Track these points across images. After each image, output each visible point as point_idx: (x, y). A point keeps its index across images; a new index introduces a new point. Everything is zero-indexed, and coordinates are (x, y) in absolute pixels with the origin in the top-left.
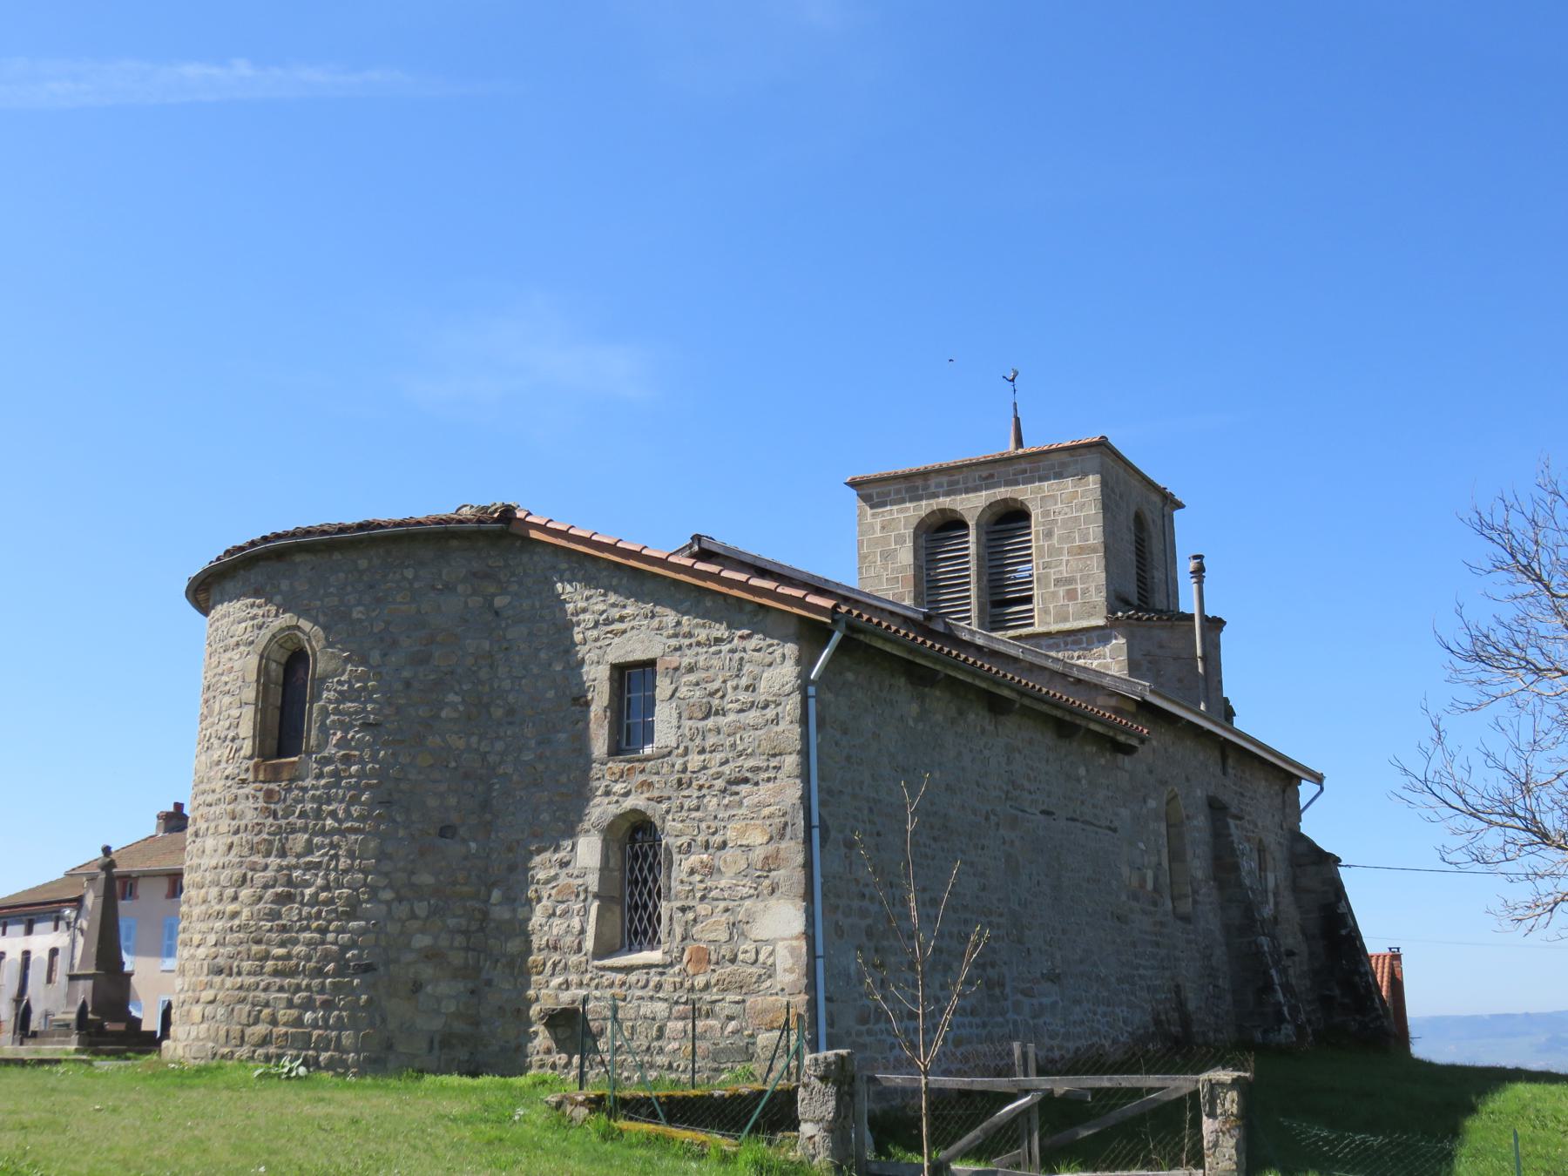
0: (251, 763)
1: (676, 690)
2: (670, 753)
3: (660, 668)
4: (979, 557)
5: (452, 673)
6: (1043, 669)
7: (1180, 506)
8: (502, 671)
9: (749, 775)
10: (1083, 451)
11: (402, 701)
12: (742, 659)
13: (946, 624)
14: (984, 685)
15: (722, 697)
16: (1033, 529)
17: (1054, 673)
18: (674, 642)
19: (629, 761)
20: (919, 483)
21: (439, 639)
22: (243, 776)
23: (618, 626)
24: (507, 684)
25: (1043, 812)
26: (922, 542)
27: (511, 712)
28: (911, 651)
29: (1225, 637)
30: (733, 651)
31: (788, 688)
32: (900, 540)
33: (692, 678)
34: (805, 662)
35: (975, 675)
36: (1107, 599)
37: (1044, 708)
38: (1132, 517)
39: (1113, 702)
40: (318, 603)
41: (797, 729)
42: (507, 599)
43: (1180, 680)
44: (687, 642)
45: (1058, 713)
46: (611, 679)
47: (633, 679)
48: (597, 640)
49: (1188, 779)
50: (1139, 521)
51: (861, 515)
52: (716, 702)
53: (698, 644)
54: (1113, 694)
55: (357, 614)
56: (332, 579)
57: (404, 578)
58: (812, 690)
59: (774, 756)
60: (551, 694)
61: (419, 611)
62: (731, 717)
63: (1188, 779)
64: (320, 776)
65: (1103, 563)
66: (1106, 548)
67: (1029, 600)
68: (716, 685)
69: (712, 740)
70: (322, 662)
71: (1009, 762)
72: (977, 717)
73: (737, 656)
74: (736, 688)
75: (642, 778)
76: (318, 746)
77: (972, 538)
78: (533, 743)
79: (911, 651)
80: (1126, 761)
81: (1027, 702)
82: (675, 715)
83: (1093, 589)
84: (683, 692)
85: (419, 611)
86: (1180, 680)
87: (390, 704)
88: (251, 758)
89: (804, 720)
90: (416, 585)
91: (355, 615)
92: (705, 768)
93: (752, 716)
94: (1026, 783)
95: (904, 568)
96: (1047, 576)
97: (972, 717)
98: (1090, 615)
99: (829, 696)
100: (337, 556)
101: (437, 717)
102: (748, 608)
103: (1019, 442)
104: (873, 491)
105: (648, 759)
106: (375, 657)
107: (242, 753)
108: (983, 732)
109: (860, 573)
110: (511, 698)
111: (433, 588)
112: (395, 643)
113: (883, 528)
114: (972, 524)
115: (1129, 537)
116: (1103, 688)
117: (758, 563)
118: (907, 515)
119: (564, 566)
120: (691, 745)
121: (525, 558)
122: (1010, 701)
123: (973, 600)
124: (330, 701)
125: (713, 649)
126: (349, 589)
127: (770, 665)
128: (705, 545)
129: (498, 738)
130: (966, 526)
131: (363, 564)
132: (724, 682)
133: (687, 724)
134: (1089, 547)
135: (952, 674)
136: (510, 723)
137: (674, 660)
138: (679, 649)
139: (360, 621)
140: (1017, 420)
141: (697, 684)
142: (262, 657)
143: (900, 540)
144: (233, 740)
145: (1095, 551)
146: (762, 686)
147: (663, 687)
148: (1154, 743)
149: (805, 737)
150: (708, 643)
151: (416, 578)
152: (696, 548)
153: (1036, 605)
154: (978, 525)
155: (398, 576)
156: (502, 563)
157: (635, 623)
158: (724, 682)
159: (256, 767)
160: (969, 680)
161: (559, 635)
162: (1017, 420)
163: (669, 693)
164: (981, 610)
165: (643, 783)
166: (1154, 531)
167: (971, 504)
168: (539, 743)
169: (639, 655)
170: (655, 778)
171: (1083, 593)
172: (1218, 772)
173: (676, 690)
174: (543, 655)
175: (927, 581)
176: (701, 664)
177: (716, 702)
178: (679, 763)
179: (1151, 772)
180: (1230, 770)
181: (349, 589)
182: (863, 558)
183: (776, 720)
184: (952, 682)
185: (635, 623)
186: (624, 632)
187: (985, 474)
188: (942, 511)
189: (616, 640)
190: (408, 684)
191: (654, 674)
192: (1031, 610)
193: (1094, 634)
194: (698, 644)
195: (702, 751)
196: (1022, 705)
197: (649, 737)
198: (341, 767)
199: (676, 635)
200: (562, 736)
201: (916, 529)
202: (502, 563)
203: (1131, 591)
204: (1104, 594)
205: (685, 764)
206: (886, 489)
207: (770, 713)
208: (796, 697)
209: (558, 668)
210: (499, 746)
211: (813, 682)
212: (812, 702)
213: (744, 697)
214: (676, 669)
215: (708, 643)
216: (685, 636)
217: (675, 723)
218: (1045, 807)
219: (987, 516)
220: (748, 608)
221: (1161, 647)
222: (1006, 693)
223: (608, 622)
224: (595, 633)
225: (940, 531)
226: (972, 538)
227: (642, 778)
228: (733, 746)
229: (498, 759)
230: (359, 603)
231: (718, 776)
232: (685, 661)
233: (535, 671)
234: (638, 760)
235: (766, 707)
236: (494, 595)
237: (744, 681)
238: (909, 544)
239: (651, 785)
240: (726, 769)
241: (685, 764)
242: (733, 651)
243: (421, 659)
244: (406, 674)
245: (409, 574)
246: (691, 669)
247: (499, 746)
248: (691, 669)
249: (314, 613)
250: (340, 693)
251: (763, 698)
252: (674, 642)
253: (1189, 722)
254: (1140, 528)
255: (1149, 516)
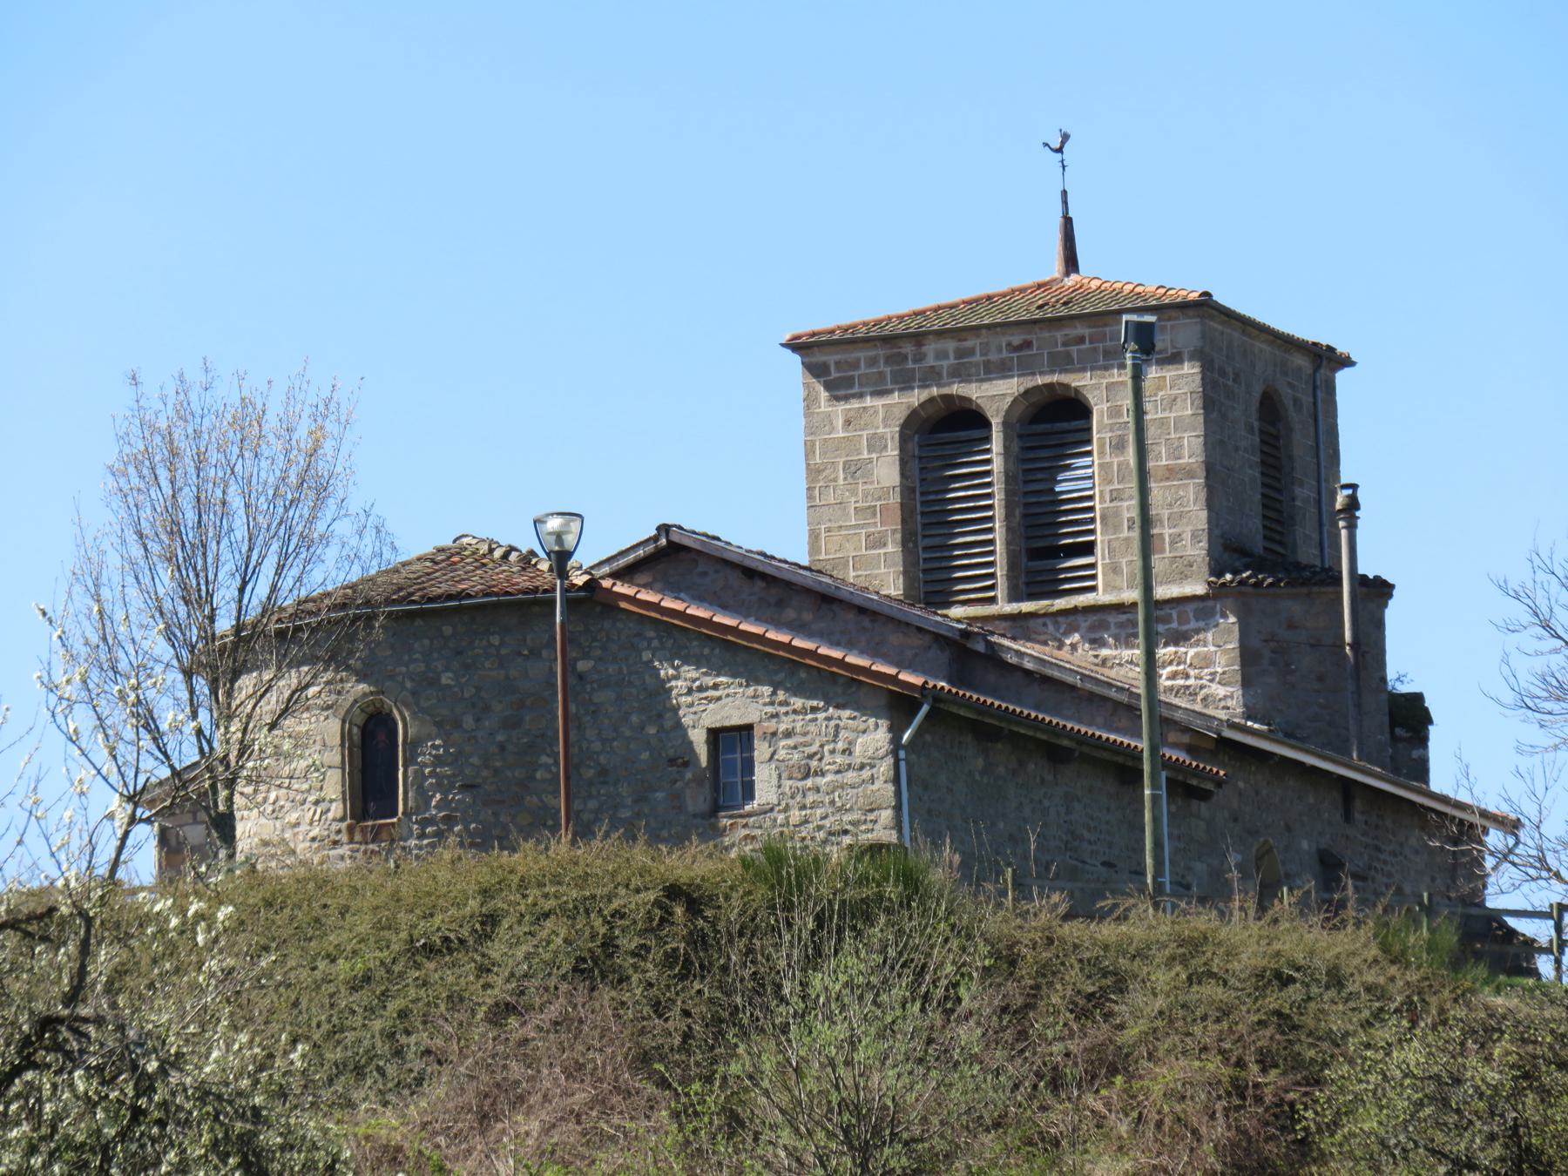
0: (344, 825)
1: (774, 753)
2: (772, 810)
3: (757, 732)
4: (1009, 478)
5: (543, 736)
6: (1105, 699)
7: (1346, 362)
8: (590, 734)
9: (849, 827)
10: (1173, 313)
11: (498, 764)
12: (837, 726)
13: (989, 643)
14: (1044, 737)
15: (820, 760)
16: (1095, 436)
17: (1118, 704)
18: (770, 709)
19: (731, 817)
20: (908, 349)
21: (528, 702)
22: (333, 837)
23: (711, 693)
24: (597, 746)
25: (1104, 864)
26: (913, 447)
27: (603, 772)
28: (980, 713)
29: (1394, 614)
30: (828, 719)
31: (882, 752)
32: (876, 444)
33: (791, 742)
34: (896, 731)
35: (1036, 728)
36: (1210, 552)
37: (1105, 755)
38: (1255, 405)
39: (1186, 739)
40: (404, 669)
41: (891, 788)
42: (591, 664)
43: (1321, 678)
44: (783, 709)
45: (1120, 759)
46: (708, 742)
47: (732, 741)
48: (691, 705)
49: (1288, 828)
50: (1270, 407)
51: (810, 401)
52: (814, 764)
53: (795, 712)
54: (1186, 729)
55: (446, 679)
56: (417, 645)
57: (491, 645)
58: (902, 754)
59: (871, 811)
60: (645, 756)
61: (507, 677)
62: (829, 778)
63: (1288, 828)
64: (422, 836)
65: (1203, 495)
66: (1208, 471)
67: (1088, 549)
68: (814, 748)
69: (810, 798)
70: (405, 726)
71: (1068, 812)
72: (1036, 767)
73: (832, 723)
74: (832, 752)
75: (747, 832)
76: (418, 808)
77: (997, 444)
78: (629, 801)
79: (980, 713)
80: (1204, 808)
81: (1085, 749)
82: (775, 776)
83: (1187, 536)
84: (782, 754)
85: (507, 677)
86: (1320, 679)
87: (487, 767)
88: (343, 819)
89: (896, 780)
90: (503, 651)
91: (444, 681)
92: (806, 822)
93: (850, 776)
94: (1086, 834)
95: (885, 492)
96: (1117, 513)
97: (1031, 766)
98: (1184, 577)
99: (913, 757)
100: (419, 622)
101: (532, 778)
102: (841, 681)
103: (1071, 262)
104: (836, 360)
105: (749, 815)
106: (468, 722)
107: (330, 815)
108: (1043, 781)
109: (810, 498)
110: (602, 759)
111: (519, 654)
112: (487, 709)
113: (848, 423)
114: (996, 422)
115: (1248, 440)
116: (1176, 723)
117: (747, 563)
118: (886, 412)
119: (651, 634)
120: (791, 802)
121: (607, 624)
122: (1071, 751)
123: (999, 547)
124: (425, 765)
125: (809, 717)
126: (435, 655)
127: (864, 732)
128: (675, 538)
129: (590, 796)
130: (986, 424)
131: (448, 630)
132: (822, 746)
133: (787, 784)
134: (1182, 468)
135: (1016, 729)
136: (604, 783)
137: (771, 725)
138: (776, 716)
139: (449, 686)
140: (1068, 223)
141: (795, 747)
142: (344, 722)
143: (876, 444)
144: (317, 803)
145: (1190, 474)
146: (858, 749)
147: (761, 750)
148: (1241, 784)
149: (898, 794)
150: (803, 711)
151: (502, 644)
152: (663, 541)
153: (1100, 557)
154: (1006, 424)
155: (485, 643)
156: (581, 628)
157: (731, 691)
158: (822, 746)
159: (351, 830)
160: (1031, 733)
161: (657, 700)
162: (1068, 223)
163: (768, 756)
164: (1012, 566)
165: (746, 837)
166: (1297, 420)
167: (996, 395)
168: (636, 801)
169: (736, 720)
170: (759, 832)
171: (1172, 543)
172: (1338, 817)
173: (774, 753)
174: (634, 719)
175: (929, 525)
176: (798, 730)
177: (814, 764)
178: (781, 818)
179: (1236, 820)
180: (1358, 816)
181: (435, 655)
182: (813, 472)
183: (872, 779)
184: (1014, 736)
185: (731, 691)
186: (719, 699)
187: (1017, 340)
188: (947, 398)
189: (711, 706)
190: (502, 748)
191: (750, 739)
192: (1092, 566)
193: (1190, 608)
194: (795, 712)
195: (803, 807)
196: (1081, 754)
197: (749, 794)
198: (443, 827)
199: (772, 703)
200: (660, 795)
201: (905, 426)
202: (581, 628)
203: (1252, 528)
204: (1204, 544)
205: (787, 818)
206: (852, 356)
207: (866, 774)
208: (890, 760)
209: (652, 730)
210: (593, 804)
211: (904, 747)
212: (903, 765)
213: (839, 759)
214: (774, 734)
215: (803, 711)
216: (781, 704)
217: (775, 781)
218: (1105, 858)
219: (1020, 409)
220: (841, 681)
221: (1291, 626)
222: (1065, 742)
223: (701, 689)
224: (689, 699)
225: (942, 434)
226: (997, 444)
227: (747, 832)
228: (832, 802)
229: (592, 816)
230: (447, 669)
231: (820, 828)
232: (782, 727)
233: (628, 733)
234: (742, 816)
235: (862, 767)
236: (576, 660)
237: (840, 745)
238: (893, 452)
239: (754, 838)
240: (827, 823)
241: (787, 818)
242: (828, 719)
243: (511, 724)
244: (500, 738)
245: (495, 640)
246: (788, 734)
247: (593, 804)
248: (788, 734)
249: (400, 678)
250: (435, 757)
251: (858, 761)
252: (770, 709)
253: (1283, 758)
254: (1273, 412)
255: (1286, 394)
